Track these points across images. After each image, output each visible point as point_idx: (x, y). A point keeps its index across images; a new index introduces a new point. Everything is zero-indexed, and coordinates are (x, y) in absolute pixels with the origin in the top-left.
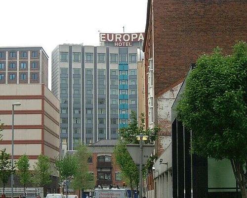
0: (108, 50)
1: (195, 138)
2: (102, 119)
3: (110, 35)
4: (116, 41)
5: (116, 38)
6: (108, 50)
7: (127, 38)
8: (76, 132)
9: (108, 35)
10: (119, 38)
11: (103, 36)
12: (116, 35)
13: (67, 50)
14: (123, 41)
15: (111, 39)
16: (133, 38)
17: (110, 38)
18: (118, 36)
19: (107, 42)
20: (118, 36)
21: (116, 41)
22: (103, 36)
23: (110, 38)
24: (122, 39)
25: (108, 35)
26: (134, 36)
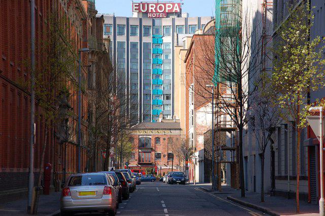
3: (143, 5)
5: (150, 8)
10: (153, 9)
11: (135, 6)
12: (150, 5)
14: (157, 12)
16: (167, 9)
20: (152, 6)
22: (135, 6)
25: (141, 5)
26: (169, 6)
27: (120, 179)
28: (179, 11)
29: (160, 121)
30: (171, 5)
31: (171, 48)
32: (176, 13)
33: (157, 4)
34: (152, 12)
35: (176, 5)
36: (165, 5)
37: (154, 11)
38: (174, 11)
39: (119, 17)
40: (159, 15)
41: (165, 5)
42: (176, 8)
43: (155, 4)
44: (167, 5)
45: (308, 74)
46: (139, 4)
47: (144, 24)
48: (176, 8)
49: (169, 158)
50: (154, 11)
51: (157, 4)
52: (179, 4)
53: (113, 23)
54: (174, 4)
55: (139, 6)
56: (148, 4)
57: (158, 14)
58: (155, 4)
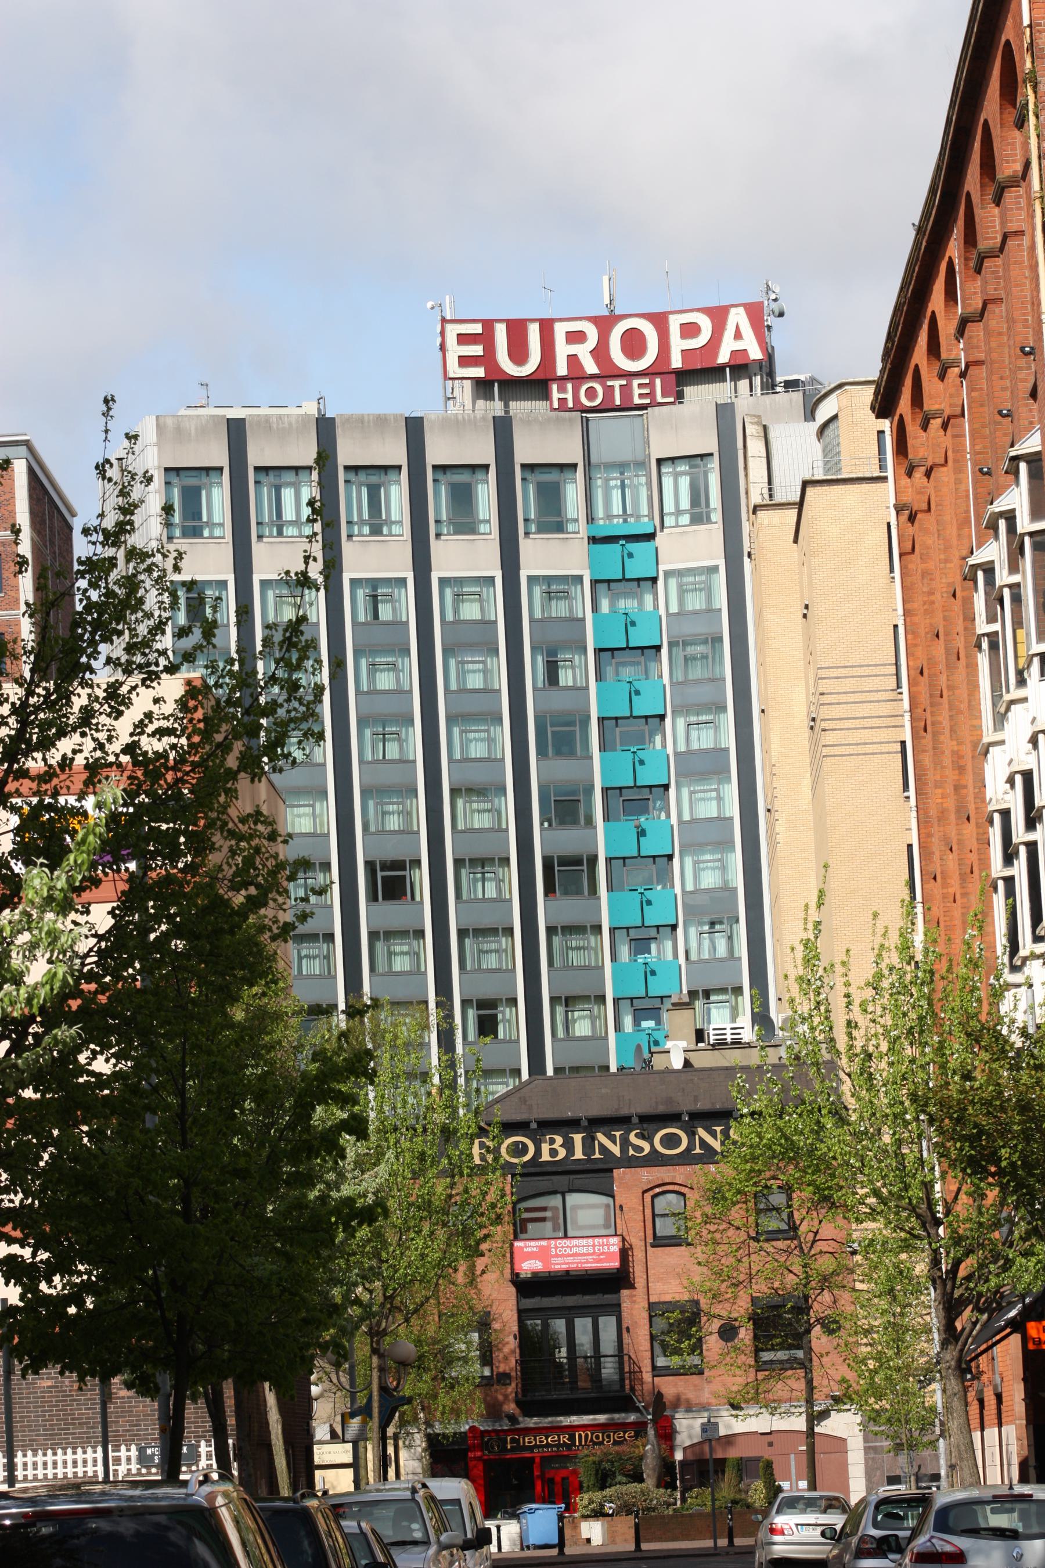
0: (503, 429)
1: (732, 956)
2: (399, 865)
3: (517, 329)
4: (562, 370)
5: (563, 350)
6: (503, 429)
7: (633, 343)
8: (487, 1026)
9: (501, 332)
10: (584, 352)
11: (463, 339)
12: (560, 330)
13: (218, 455)
14: (609, 372)
15: (519, 354)
16: (678, 345)
17: (518, 352)
18: (576, 337)
19: (312, 715)
20: (576, 337)
21: (562, 370)
22: (463, 339)
23: (518, 352)
24: (600, 353)
25: (501, 332)
26: (690, 330)
27: (346, 1070)
28: (755, 353)
29: (677, 1064)
30: (705, 324)
31: (722, 601)
32: (740, 368)
33: (604, 324)
34: (577, 375)
35: (738, 317)
36: (660, 321)
37: (591, 367)
38: (723, 358)
39: (348, 420)
40: (626, 390)
41: (660, 321)
42: (738, 335)
43: (595, 320)
44: (675, 323)
45: (925, 599)
46: (488, 325)
47: (525, 451)
48: (738, 335)
49: (763, 1338)
50: (591, 367)
51: (604, 324)
52: (755, 312)
53: (721, 563)
54: (719, 315)
55: (486, 338)
56: (547, 327)
57: (617, 384)
58: (595, 320)
